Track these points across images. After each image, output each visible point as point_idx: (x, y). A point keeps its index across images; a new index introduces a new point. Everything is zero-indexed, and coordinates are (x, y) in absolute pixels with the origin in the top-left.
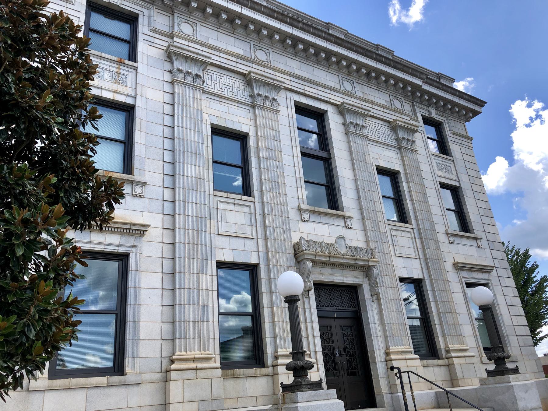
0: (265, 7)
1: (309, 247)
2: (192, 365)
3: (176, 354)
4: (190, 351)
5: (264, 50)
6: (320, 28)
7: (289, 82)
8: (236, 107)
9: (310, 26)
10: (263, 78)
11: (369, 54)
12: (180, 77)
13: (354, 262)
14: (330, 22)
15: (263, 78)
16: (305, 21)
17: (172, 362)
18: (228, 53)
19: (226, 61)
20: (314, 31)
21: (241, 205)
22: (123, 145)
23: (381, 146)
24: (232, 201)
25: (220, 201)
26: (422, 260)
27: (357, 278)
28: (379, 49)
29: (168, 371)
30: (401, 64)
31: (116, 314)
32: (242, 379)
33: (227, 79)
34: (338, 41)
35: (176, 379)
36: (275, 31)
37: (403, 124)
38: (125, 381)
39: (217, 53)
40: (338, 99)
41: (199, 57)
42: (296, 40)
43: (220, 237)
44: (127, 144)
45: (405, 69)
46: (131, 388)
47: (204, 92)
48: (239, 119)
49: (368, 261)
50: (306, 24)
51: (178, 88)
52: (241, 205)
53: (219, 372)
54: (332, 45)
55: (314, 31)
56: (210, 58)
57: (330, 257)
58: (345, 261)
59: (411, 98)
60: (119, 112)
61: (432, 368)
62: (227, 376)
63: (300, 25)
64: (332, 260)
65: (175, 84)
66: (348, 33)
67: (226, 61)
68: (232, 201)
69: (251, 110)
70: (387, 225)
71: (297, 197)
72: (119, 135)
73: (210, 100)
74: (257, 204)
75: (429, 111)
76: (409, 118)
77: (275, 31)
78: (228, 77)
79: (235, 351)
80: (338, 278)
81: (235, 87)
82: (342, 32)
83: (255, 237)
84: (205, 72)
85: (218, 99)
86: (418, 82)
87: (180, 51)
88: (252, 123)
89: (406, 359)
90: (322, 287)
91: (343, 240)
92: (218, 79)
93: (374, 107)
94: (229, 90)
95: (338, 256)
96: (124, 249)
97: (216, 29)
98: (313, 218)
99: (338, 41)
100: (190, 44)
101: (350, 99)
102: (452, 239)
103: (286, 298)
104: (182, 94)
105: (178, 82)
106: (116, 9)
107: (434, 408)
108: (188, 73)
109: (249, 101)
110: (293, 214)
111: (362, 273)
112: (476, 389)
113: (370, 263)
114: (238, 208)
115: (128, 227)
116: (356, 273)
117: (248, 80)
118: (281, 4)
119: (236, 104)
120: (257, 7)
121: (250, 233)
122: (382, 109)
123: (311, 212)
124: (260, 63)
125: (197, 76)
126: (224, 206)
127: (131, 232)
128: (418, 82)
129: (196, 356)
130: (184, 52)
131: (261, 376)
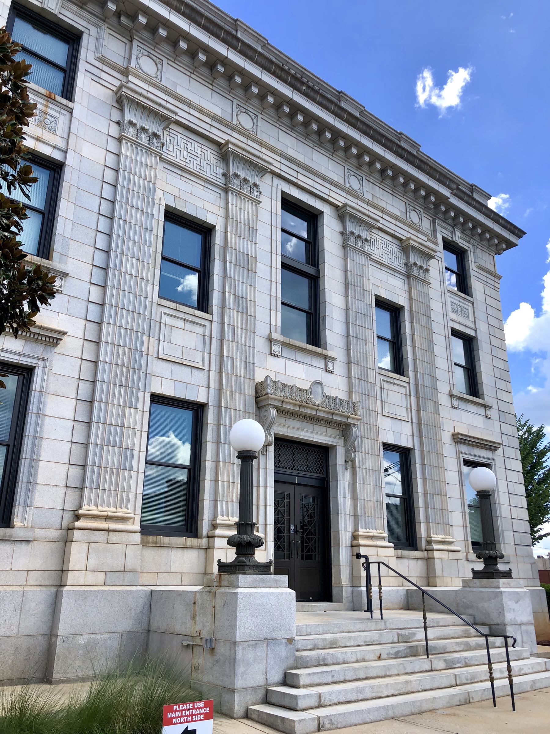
3: (84, 507)
4: (232, 516)
6: (329, 96)
9: (317, 92)
10: (244, 153)
11: (389, 144)
12: (131, 133)
14: (343, 91)
15: (244, 153)
17: (77, 517)
23: (386, 270)
24: (182, 315)
25: (383, 380)
28: (402, 140)
29: (70, 529)
31: (8, 446)
35: (79, 540)
37: (417, 245)
38: (11, 536)
40: (339, 198)
41: (161, 109)
42: (296, 108)
46: (18, 545)
48: (204, 205)
49: (348, 417)
57: (300, 406)
58: (319, 414)
62: (147, 543)
63: (304, 88)
64: (302, 410)
65: (124, 141)
66: (268, 43)
68: (182, 315)
70: (377, 374)
75: (452, 233)
76: (426, 239)
78: (196, 143)
80: (307, 434)
81: (205, 160)
82: (357, 108)
83: (206, 368)
85: (179, 172)
88: (222, 212)
89: (377, 546)
90: (284, 444)
95: (311, 406)
96: (28, 360)
97: (189, 74)
98: (286, 352)
100: (151, 89)
102: (455, 403)
108: (143, 129)
109: (221, 181)
113: (350, 421)
114: (188, 326)
116: (330, 431)
117: (224, 153)
120: (250, 53)
121: (201, 362)
125: (155, 135)
127: (40, 338)
129: (110, 514)
130: (142, 99)
131: (192, 548)
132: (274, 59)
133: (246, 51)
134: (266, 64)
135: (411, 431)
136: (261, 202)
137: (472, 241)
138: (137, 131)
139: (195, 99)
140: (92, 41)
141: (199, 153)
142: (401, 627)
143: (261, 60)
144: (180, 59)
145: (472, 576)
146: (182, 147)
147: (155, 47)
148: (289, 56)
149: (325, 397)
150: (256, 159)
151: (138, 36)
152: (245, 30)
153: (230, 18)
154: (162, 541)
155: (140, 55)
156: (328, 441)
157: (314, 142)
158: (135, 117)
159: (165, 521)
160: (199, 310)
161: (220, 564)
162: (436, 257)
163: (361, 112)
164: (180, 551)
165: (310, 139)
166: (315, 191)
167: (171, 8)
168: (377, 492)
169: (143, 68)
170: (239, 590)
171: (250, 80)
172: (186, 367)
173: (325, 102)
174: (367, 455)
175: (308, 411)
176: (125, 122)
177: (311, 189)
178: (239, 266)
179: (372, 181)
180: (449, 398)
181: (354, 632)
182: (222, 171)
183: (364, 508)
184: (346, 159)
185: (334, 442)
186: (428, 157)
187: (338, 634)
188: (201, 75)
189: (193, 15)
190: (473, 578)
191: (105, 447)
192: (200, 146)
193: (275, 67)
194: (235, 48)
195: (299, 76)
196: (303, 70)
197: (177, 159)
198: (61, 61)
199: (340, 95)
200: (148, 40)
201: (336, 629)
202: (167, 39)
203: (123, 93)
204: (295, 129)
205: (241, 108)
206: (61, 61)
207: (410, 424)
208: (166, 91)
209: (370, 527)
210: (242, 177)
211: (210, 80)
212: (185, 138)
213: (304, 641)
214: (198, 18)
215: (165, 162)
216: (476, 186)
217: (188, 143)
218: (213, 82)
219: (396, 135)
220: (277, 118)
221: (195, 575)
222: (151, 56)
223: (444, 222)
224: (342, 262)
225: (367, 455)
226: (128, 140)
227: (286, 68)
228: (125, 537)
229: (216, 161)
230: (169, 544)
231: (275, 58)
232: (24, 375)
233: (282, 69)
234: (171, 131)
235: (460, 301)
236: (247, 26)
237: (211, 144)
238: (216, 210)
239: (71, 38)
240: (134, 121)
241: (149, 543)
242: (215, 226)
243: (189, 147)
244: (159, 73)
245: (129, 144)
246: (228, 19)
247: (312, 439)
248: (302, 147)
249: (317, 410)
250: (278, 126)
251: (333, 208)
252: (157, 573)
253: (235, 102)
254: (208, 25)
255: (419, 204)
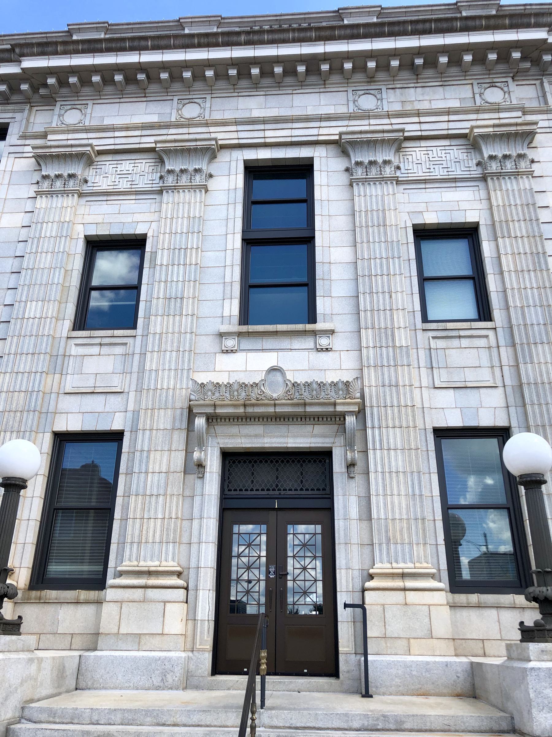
0: (106, 40)
1: (205, 394)
2: (399, 583)
3: (376, 566)
4: (397, 562)
6: (324, 24)
7: (224, 135)
8: (134, 201)
9: (309, 29)
10: (176, 144)
11: (396, 28)
13: (300, 409)
15: (176, 144)
16: (295, 26)
17: (371, 577)
18: (127, 128)
20: (270, 37)
21: (111, 344)
24: (98, 341)
25: (434, 338)
27: (324, 436)
28: (461, 9)
29: (364, 590)
30: (530, 15)
31: (508, 509)
32: (54, 605)
34: (323, 33)
36: (390, 56)
37: (491, 129)
39: (110, 134)
40: (331, 131)
41: (74, 149)
42: (244, 65)
43: (437, 391)
45: (136, 43)
48: (460, 205)
51: (359, 189)
52: (111, 344)
53: (442, 598)
55: (270, 37)
56: (403, 131)
57: (245, 406)
58: (278, 409)
61: (494, 612)
62: (28, 599)
63: (243, 38)
64: (250, 410)
65: (489, 179)
66: (224, 18)
68: (98, 341)
73: (440, 190)
74: (499, 330)
76: (519, 114)
77: (390, 56)
78: (439, 148)
79: (73, 562)
80: (274, 440)
81: (454, 159)
82: (369, 14)
84: (401, 154)
85: (105, 198)
86: (132, 58)
87: (47, 150)
89: (405, 589)
90: (293, 458)
91: (278, 374)
92: (423, 156)
94: (441, 166)
95: (266, 402)
97: (118, 100)
98: (246, 344)
99: (323, 33)
100: (70, 136)
104: (513, 190)
107: (459, 696)
108: (506, 157)
110: (207, 344)
112: (498, 666)
113: (339, 409)
114: (105, 350)
116: (319, 429)
117: (472, 142)
118: (144, 23)
120: (163, 42)
124: (190, 123)
125: (521, 156)
126: (441, 343)
129: (406, 571)
130: (53, 150)
131: (87, 602)
136: (533, 171)
138: (500, 162)
141: (443, 155)
142: (298, 725)
143: (178, 42)
144: (104, 93)
145: (520, 637)
146: (423, 159)
147: (100, 95)
151: (59, 97)
152: (191, 22)
153: (173, 22)
154: (48, 597)
158: (494, 150)
159: (90, 572)
160: (481, 321)
161: (524, 629)
163: (107, 31)
164: (72, 607)
165: (284, 86)
167: (71, 54)
168: (415, 504)
169: (489, 101)
170: (531, 665)
172: (100, 394)
173: (276, 36)
174: (392, 452)
175: (258, 410)
176: (485, 159)
177: (289, 139)
179: (398, 86)
181: (185, 725)
182: (475, 162)
183: (387, 532)
184: (346, 81)
187: (150, 728)
190: (521, 641)
191: (389, 497)
193: (510, 19)
194: (146, 48)
195: (276, 27)
196: (278, 18)
199: (339, 14)
200: (386, 79)
201: (148, 719)
203: (475, 134)
204: (260, 85)
208: (236, 122)
209: (400, 559)
211: (141, 93)
213: (48, 731)
214: (98, 46)
215: (86, 196)
217: (428, 152)
218: (145, 94)
219: (449, 9)
221: (89, 636)
222: (75, 107)
223: (8, 104)
225: (392, 452)
227: (257, 28)
228: (427, 597)
229: (466, 154)
230: (56, 599)
231: (239, 27)
232: (502, 436)
233: (255, 32)
234: (99, 163)
236: (191, 18)
237: (147, 154)
240: (494, 154)
241: (31, 599)
242: (478, 223)
244: (507, 95)
245: (512, 177)
246: (171, 24)
248: (273, 101)
249: (275, 405)
250: (236, 94)
251: (333, 146)
252: (40, 634)
254: (109, 45)
255: (501, 73)
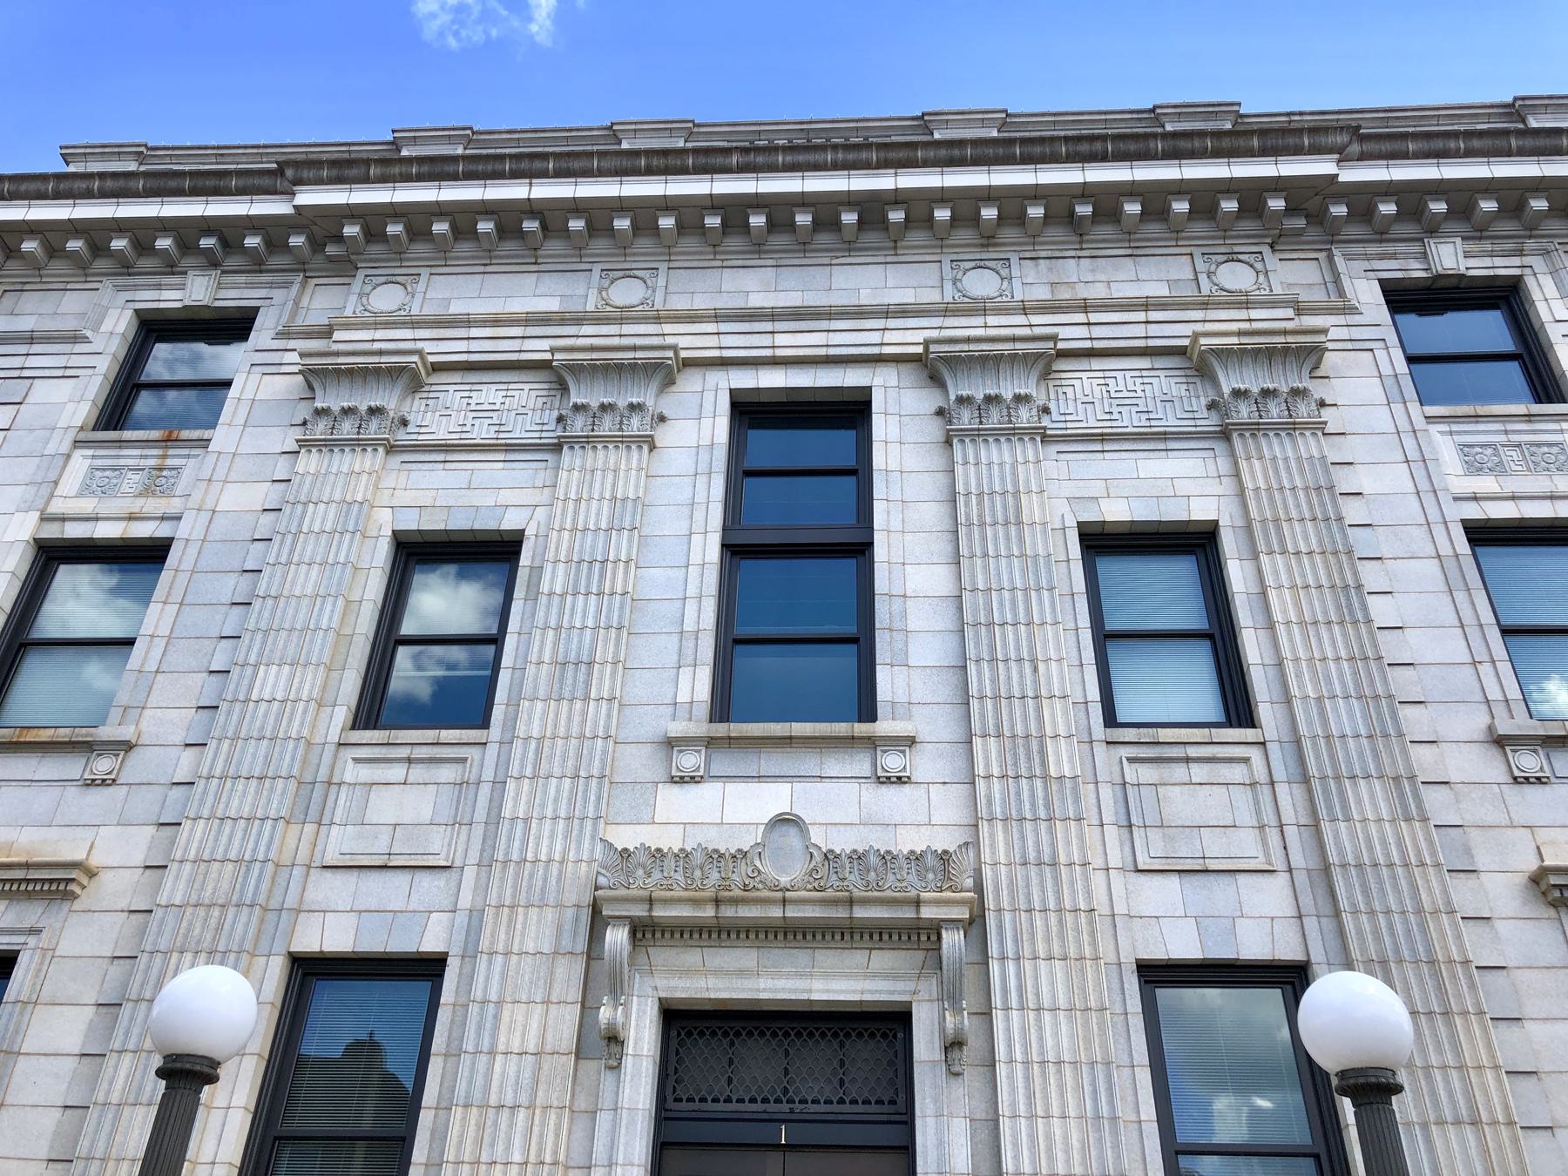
1: (630, 874)
5: (637, 273)
7: (692, 340)
11: (1038, 150)
12: (1244, 412)
13: (841, 913)
14: (1158, 103)
18: (496, 322)
19: (488, 345)
20: (789, 158)
22: (1207, 644)
23: (1080, 447)
24: (403, 752)
25: (1131, 760)
26: (1301, 878)
28: (1164, 119)
31: (1317, 1157)
33: (1126, 377)
37: (1235, 340)
40: (908, 337)
43: (1143, 878)
44: (1218, 636)
47: (1046, 439)
48: (1182, 486)
50: (848, 147)
54: (1065, 169)
55: (789, 158)
57: (717, 902)
58: (792, 912)
59: (1313, 233)
60: (143, 566)
63: (735, 159)
64: (728, 912)
65: (1235, 435)
67: (488, 345)
68: (403, 752)
69: (1220, 447)
70: (1100, 750)
71: (1479, 697)
72: (1191, 615)
75: (1424, 256)
77: (1027, 198)
78: (1128, 374)
80: (781, 983)
81: (1162, 395)
84: (1051, 384)
85: (441, 457)
86: (515, 191)
88: (1228, 486)
91: (793, 831)
92: (1097, 390)
93: (1094, 317)
94: (1134, 409)
95: (766, 893)
97: (482, 269)
98: (723, 763)
100: (379, 334)
101: (979, 321)
102: (1529, 762)
103: (168, 1058)
104: (1286, 459)
105: (964, 434)
106: (207, 315)
108: (1266, 393)
109: (1210, 422)
111: (920, 955)
113: (927, 913)
114: (417, 773)
115: (19, 874)
116: (882, 959)
117: (1196, 363)
119: (501, 457)
120: (576, 164)
121: (1261, 856)
122: (1141, 316)
123: (711, 743)
125: (1296, 393)
128: (515, 191)
132: (725, 144)
133: (437, 170)
134: (708, 161)
135: (1291, 900)
137: (1530, 244)
139: (518, 306)
140: (1548, 283)
148: (567, 126)
149: (818, 857)
150: (630, 355)
155: (1213, 268)
156: (871, 992)
157: (827, 250)
160: (1231, 726)
162: (1330, 345)
166: (832, 351)
168: (1100, 1140)
171: (779, 209)
172: (399, 872)
174: (1047, 1016)
178: (1280, 587)
179: (1043, 254)
180: (1494, 751)
182: (1203, 401)
185: (904, 992)
186: (1289, 114)
188: (508, 257)
189: (437, 169)
192: (1137, 373)
194: (543, 174)
197: (1091, 421)
198: (1507, 344)
199: (924, 122)
202: (772, 226)
205: (1214, 258)
206: (1504, 341)
207: (1282, 879)
210: (595, 404)
212: (1100, 374)
216: (1523, 99)
220: (711, 249)
224: (942, 479)
225: (1047, 1016)
226: (1243, 428)
232: (1292, 983)
233: (758, 150)
235: (1506, 432)
238: (1214, 488)
239: (1505, 296)
243: (1112, 388)
247: (805, 996)
250: (719, 263)
253: (1197, 252)
254: (472, 167)
